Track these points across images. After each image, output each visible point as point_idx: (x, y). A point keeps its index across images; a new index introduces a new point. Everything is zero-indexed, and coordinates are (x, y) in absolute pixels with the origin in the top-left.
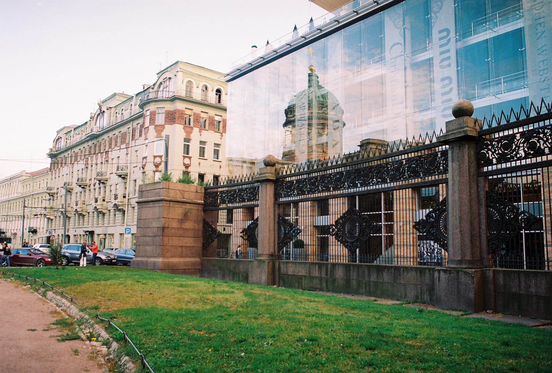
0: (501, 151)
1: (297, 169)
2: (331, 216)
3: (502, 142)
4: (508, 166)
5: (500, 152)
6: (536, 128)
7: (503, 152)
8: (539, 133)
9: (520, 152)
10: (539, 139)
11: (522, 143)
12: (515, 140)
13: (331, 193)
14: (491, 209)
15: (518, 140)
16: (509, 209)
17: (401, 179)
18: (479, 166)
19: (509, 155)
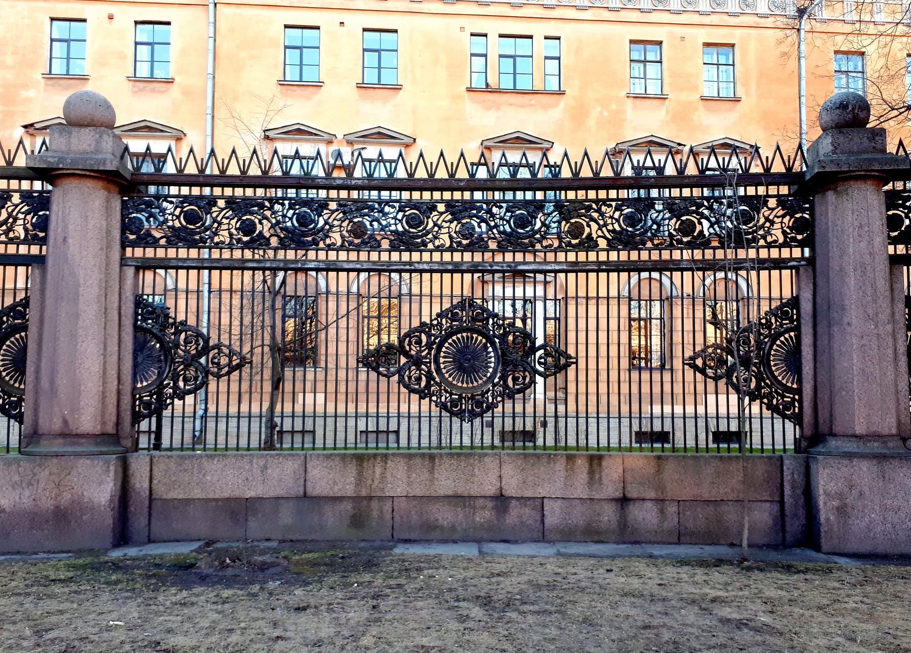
4: (158, 256)
6: (260, 198)
8: (589, 208)
10: (373, 221)
11: (23, 213)
15: (17, 206)
17: (644, 244)
19: (419, 237)
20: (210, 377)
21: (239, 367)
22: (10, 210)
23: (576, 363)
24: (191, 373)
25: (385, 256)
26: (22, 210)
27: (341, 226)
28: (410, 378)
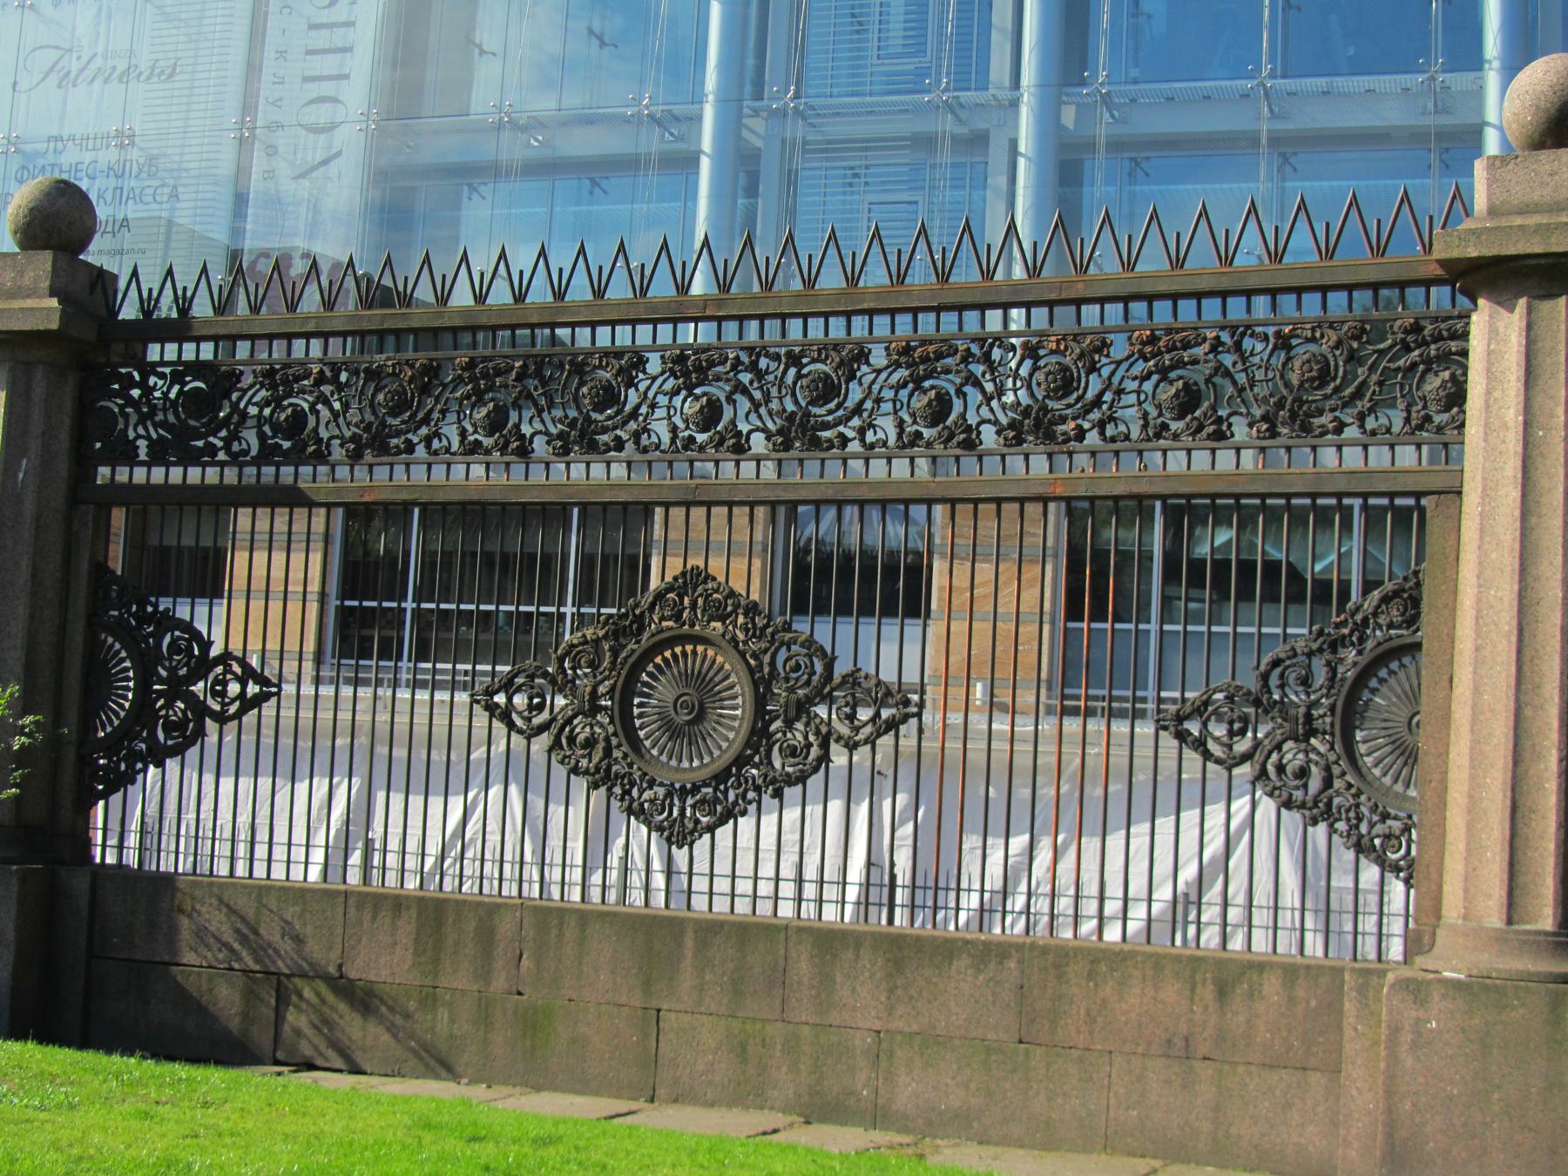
0: (176, 414)
1: (580, 279)
2: (239, 605)
3: (184, 384)
5: (171, 418)
7: (183, 423)
9: (654, 426)
11: (255, 404)
12: (864, 368)
13: (748, 468)
14: (110, 640)
15: (879, 372)
16: (174, 642)
18: (83, 464)
20: (834, 747)
21: (259, 700)
22: (867, 380)
23: (919, 715)
24: (797, 736)
25: (140, 475)
26: (255, 400)
27: (1138, 392)
28: (1281, 769)
